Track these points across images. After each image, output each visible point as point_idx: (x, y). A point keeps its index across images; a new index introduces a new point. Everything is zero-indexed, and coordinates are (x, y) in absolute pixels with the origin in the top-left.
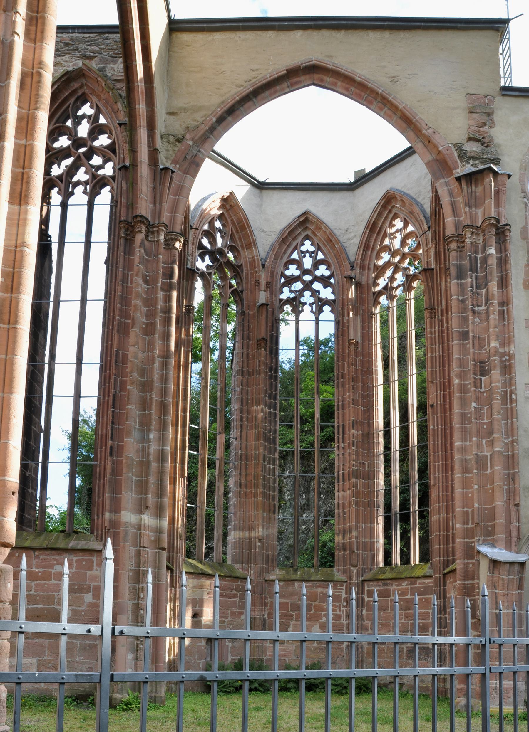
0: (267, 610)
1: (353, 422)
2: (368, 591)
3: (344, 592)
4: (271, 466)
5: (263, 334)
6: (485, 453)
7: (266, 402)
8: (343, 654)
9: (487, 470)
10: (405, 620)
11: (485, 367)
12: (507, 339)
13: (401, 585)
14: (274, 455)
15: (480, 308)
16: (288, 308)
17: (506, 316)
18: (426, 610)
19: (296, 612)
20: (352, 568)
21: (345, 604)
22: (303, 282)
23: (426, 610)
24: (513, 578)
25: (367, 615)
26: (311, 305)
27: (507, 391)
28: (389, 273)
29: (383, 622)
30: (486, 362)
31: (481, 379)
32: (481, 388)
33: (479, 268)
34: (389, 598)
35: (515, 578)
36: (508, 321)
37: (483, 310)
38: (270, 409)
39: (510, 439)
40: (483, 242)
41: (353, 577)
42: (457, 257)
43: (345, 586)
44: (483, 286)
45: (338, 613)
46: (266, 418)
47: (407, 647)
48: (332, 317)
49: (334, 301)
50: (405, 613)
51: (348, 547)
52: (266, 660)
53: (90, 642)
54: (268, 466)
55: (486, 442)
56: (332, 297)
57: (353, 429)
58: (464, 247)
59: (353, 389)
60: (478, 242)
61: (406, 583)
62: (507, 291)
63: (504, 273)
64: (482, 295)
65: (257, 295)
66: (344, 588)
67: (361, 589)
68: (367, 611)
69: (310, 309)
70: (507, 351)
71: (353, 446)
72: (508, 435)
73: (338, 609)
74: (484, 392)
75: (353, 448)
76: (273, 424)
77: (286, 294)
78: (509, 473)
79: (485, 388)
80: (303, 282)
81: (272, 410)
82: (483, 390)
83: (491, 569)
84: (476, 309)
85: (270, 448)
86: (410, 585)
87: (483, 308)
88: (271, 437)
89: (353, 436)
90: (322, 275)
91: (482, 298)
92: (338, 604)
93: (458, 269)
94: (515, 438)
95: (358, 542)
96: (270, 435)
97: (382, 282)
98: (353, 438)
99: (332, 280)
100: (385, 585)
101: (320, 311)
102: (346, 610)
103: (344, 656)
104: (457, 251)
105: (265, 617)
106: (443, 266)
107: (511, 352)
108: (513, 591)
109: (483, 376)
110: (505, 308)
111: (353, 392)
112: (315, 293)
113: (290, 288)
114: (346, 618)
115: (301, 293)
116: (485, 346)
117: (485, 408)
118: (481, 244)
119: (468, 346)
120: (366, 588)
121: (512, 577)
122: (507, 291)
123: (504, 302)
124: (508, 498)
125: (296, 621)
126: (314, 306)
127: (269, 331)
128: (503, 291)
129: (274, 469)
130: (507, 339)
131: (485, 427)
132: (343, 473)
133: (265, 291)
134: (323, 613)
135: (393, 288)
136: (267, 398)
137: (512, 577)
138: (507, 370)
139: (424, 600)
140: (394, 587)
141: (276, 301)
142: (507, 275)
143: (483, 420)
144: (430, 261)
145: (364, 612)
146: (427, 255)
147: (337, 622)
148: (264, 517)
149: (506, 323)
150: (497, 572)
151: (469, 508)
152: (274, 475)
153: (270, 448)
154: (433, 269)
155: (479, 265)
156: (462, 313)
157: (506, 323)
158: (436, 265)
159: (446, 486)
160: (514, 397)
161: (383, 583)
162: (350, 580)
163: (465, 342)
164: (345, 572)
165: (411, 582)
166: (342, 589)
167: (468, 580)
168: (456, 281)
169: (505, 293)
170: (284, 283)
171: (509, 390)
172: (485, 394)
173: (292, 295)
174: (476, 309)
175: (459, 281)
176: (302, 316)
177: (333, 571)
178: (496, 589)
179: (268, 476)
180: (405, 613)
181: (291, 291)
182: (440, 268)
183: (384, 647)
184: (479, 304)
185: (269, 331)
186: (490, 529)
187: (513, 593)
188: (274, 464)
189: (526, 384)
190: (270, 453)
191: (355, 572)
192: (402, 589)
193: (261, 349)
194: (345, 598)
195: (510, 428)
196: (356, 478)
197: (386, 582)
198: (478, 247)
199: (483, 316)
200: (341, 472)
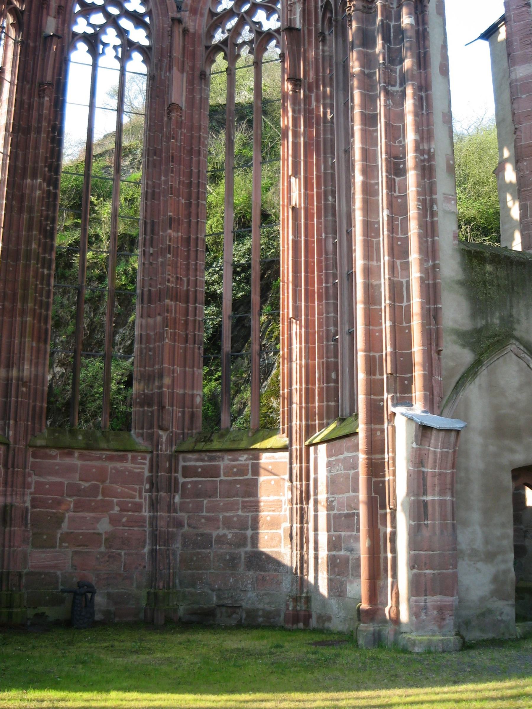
0: (31, 494)
1: (171, 218)
2: (184, 467)
3: (146, 468)
4: (46, 272)
5: (49, 78)
6: (400, 279)
7: (45, 175)
8: (143, 564)
9: (402, 302)
10: (242, 512)
11: (399, 164)
12: (425, 133)
13: (237, 460)
14: (50, 255)
15: (394, 89)
16: (82, 47)
17: (425, 104)
18: (276, 498)
19: (75, 498)
20: (161, 433)
21: (148, 486)
22: (108, 15)
23: (276, 498)
24: (448, 452)
25: (181, 503)
26: (115, 47)
27: (426, 199)
28: (231, 24)
29: (208, 514)
30: (401, 158)
31: (394, 179)
32: (395, 192)
33: (392, 38)
34: (218, 479)
35: (450, 451)
36: (427, 111)
37: (397, 91)
38: (48, 185)
39: (431, 263)
40: (397, 7)
41: (162, 445)
42: (362, 18)
43: (148, 459)
44: (397, 62)
45: (137, 500)
46: (43, 197)
47: (246, 553)
48: (144, 69)
49: (149, 48)
50: (243, 502)
51: (156, 400)
52: (27, 574)
53: (52, 511)
54: (41, 270)
55: (401, 263)
56: (146, 42)
57: (170, 228)
58: (371, 8)
59: (172, 172)
60: (391, 6)
61: (246, 456)
62: (426, 73)
63: (422, 51)
64: (396, 73)
65: (44, 21)
66: (147, 462)
67: (173, 465)
68: (182, 496)
69: (114, 53)
70: (426, 147)
71: (169, 253)
72: (428, 257)
73: (137, 494)
74: (398, 197)
75: (169, 256)
76: (52, 209)
77: (219, 36)
78: (430, 308)
79: (399, 192)
80: (108, 15)
81: (51, 188)
82: (397, 194)
83: (419, 438)
84: (390, 88)
85: (45, 243)
86: (251, 459)
87: (397, 88)
88: (48, 228)
89: (170, 240)
90: (135, 11)
91: (396, 77)
92: (137, 487)
93: (363, 34)
94: (437, 262)
95: (172, 394)
96: (47, 225)
97: (219, 36)
98: (170, 241)
99: (147, 20)
100: (211, 459)
101: (124, 59)
102: (150, 497)
103: (145, 567)
104: (363, 12)
105: (26, 505)
106: (313, 28)
107: (432, 150)
108: (445, 469)
109: (397, 176)
110: (423, 94)
111: (172, 177)
112: (122, 33)
113: (87, 19)
114: (149, 508)
115: (236, 31)
116: (400, 137)
117: (400, 218)
118: (395, 9)
119: (375, 134)
120: (181, 463)
121: (446, 450)
122: (426, 73)
123: (422, 86)
124: (429, 343)
125: (74, 512)
126: (120, 50)
127: (55, 74)
128: (420, 73)
129: (49, 275)
130: (425, 133)
131: (399, 243)
132: (150, 291)
133: (55, 17)
134: (115, 500)
135: (237, 45)
136: (47, 169)
137: (446, 450)
138: (427, 173)
139: (273, 482)
140: (226, 462)
141: (69, 34)
142: (425, 53)
143: (397, 234)
144: (295, 19)
145: (177, 499)
146: (291, 11)
147: (136, 514)
148: (32, 347)
149: (424, 112)
150: (427, 443)
151: (377, 352)
152: (49, 284)
153: (45, 243)
154: (298, 30)
155: (392, 35)
156: (368, 91)
157: (424, 112)
158: (304, 25)
159: (11, 339)
160: (435, 208)
161: (208, 456)
162: (157, 451)
163: (371, 129)
164: (151, 437)
165: (253, 455)
166: (145, 464)
167: (375, 453)
168: (361, 49)
169: (423, 75)
170: (79, 12)
171: (428, 198)
172: (399, 200)
173: (90, 31)
174: (390, 88)
175: (365, 50)
176: (102, 61)
177: (130, 436)
178: (423, 466)
179: (40, 286)
180: (243, 502)
181: (89, 24)
182: (309, 31)
183: (210, 553)
184: (393, 83)
185: (55, 74)
186: (406, 382)
187: (446, 473)
188: (49, 269)
189: (444, 194)
190: (45, 252)
191: (164, 438)
192: (239, 465)
193: (43, 97)
194: (148, 477)
195: (430, 249)
196: (171, 300)
197: (214, 454)
198: (391, 12)
199: (397, 98)
200: (146, 289)
